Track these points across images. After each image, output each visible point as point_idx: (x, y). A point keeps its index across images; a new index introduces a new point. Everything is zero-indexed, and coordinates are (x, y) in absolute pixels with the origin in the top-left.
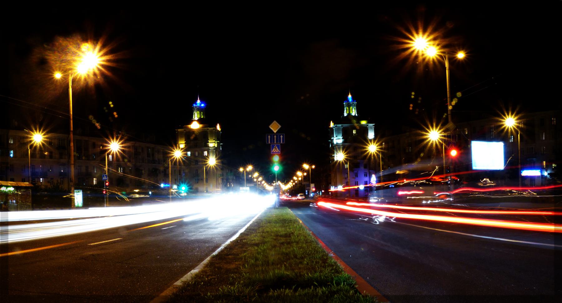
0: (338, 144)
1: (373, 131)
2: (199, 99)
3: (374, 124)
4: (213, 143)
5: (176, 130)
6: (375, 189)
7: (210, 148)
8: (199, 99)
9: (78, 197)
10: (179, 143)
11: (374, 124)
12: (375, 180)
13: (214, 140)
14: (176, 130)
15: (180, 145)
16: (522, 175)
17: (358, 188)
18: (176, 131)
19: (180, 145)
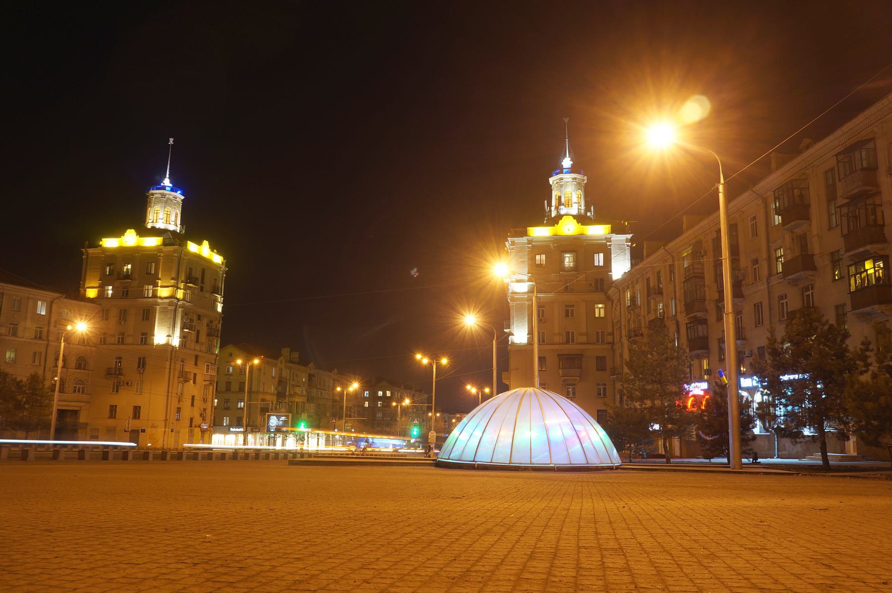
0: (516, 296)
1: (628, 256)
2: (167, 176)
3: (629, 236)
4: (168, 287)
5: (83, 250)
6: (307, 456)
7: (159, 301)
8: (167, 176)
9: (402, 387)
10: (87, 285)
11: (629, 236)
12: (223, 435)
13: (172, 279)
14: (83, 250)
15: (87, 290)
16: (129, 231)
17: (694, 396)
18: (82, 253)
19: (87, 290)
